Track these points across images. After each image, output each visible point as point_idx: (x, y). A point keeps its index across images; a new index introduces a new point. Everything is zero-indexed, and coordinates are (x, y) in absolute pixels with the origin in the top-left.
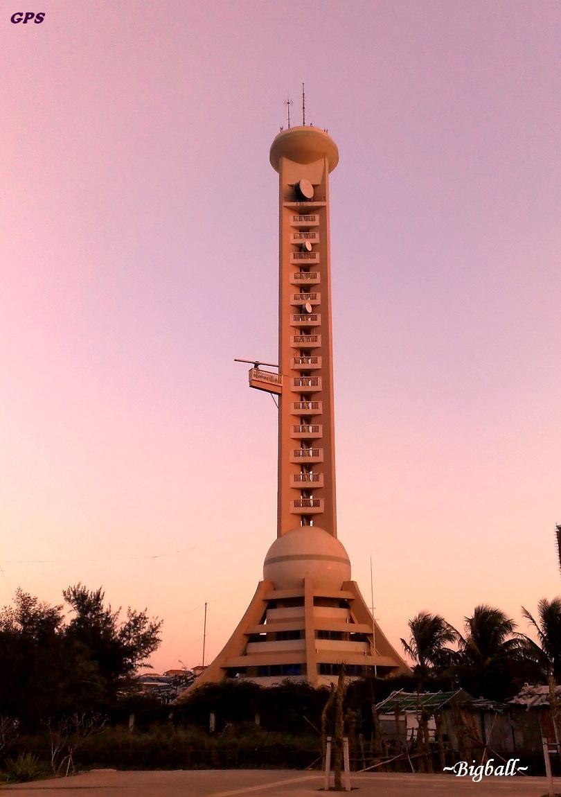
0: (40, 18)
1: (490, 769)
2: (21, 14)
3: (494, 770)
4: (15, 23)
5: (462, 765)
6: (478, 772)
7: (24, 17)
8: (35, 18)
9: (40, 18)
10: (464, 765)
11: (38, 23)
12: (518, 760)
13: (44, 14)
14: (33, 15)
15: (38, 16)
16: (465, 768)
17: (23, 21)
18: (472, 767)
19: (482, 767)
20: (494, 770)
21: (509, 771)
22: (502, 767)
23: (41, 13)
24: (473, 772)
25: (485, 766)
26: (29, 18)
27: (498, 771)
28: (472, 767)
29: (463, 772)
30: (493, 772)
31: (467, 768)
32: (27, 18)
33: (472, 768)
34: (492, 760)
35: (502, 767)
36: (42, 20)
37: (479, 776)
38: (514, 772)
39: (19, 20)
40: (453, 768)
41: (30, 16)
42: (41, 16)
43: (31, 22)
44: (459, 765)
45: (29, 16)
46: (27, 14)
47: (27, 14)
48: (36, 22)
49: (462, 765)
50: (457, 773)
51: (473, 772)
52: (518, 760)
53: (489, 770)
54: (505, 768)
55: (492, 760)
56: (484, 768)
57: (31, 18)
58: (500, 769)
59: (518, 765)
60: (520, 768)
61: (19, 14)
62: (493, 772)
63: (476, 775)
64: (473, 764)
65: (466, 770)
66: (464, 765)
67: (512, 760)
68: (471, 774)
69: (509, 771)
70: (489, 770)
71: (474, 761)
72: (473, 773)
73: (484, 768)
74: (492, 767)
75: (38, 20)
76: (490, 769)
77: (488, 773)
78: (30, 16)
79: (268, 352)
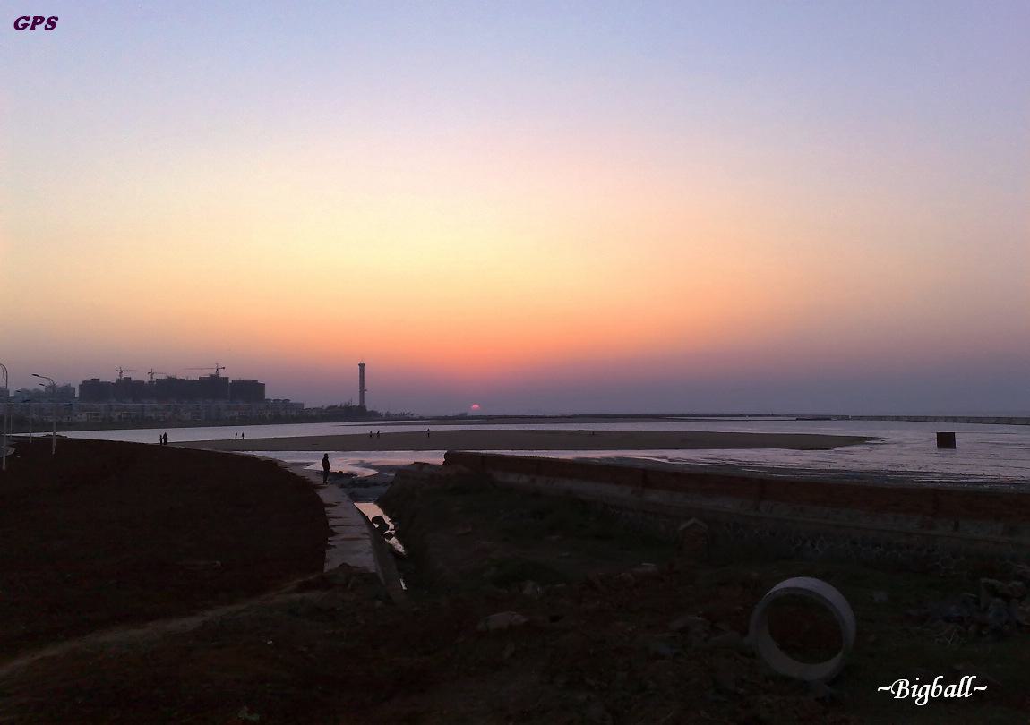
0: (52, 23)
1: (938, 689)
2: (27, 18)
3: (944, 690)
4: (20, 29)
5: (901, 684)
6: (923, 693)
7: (30, 22)
8: (45, 23)
9: (52, 23)
10: (904, 684)
11: (49, 29)
12: (975, 677)
13: (57, 19)
14: (42, 19)
15: (49, 21)
16: (905, 688)
17: (29, 27)
18: (915, 687)
19: (928, 686)
20: (944, 690)
21: (963, 691)
22: (954, 686)
23: (53, 17)
24: (917, 693)
25: (932, 685)
26: (38, 24)
27: (949, 692)
28: (915, 687)
29: (903, 692)
30: (943, 693)
31: (909, 687)
32: (35, 23)
33: (915, 687)
34: (941, 677)
35: (954, 686)
36: (54, 25)
37: (924, 697)
38: (969, 693)
39: (25, 26)
40: (890, 687)
41: (39, 21)
42: (53, 20)
43: (40, 28)
44: (898, 684)
45: (38, 20)
46: (36, 18)
47: (36, 18)
48: (46, 28)
49: (901, 684)
50: (896, 694)
51: (917, 693)
52: (975, 677)
53: (937, 690)
54: (957, 688)
55: (941, 677)
56: (931, 688)
57: (40, 23)
58: (951, 689)
59: (974, 683)
60: (977, 688)
61: (24, 17)
62: (943, 693)
63: (920, 696)
64: (916, 683)
65: (908, 691)
66: (904, 684)
67: (967, 677)
68: (913, 695)
69: (963, 691)
70: (937, 690)
71: (918, 679)
72: (916, 693)
73: (931, 688)
74: (941, 687)
75: (49, 26)
76: (938, 689)
77: (936, 694)
78: (39, 21)
79: (392, 412)
